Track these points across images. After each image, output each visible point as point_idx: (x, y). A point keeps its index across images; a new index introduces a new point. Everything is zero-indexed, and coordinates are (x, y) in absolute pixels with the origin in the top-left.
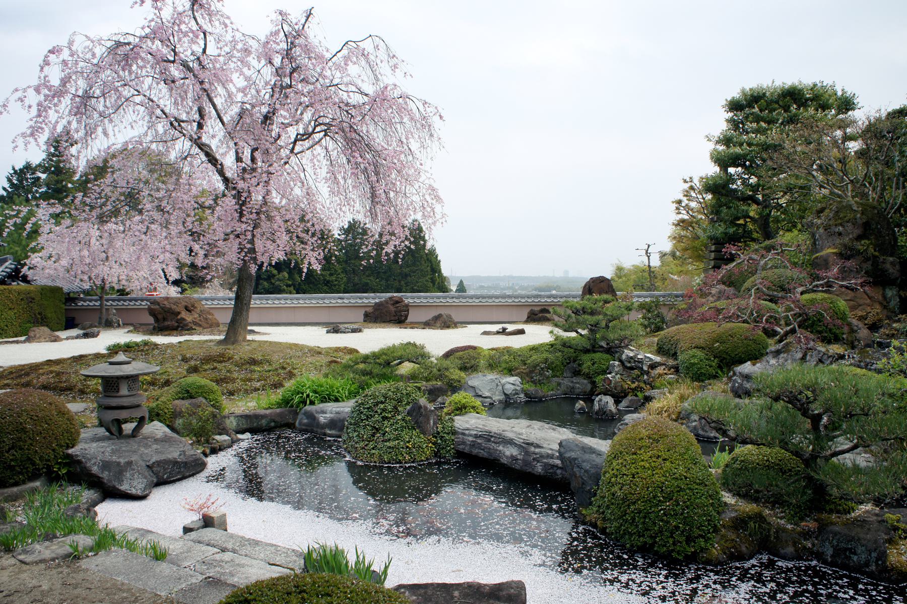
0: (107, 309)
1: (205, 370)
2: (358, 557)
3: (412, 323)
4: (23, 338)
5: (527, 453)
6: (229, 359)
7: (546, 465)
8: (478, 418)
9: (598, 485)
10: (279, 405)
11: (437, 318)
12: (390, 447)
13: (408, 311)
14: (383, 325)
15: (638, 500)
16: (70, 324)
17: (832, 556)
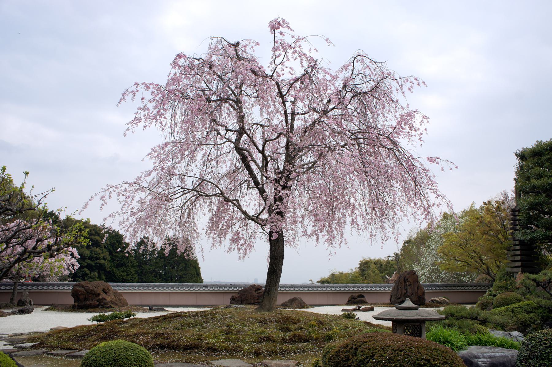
11: (293, 301)
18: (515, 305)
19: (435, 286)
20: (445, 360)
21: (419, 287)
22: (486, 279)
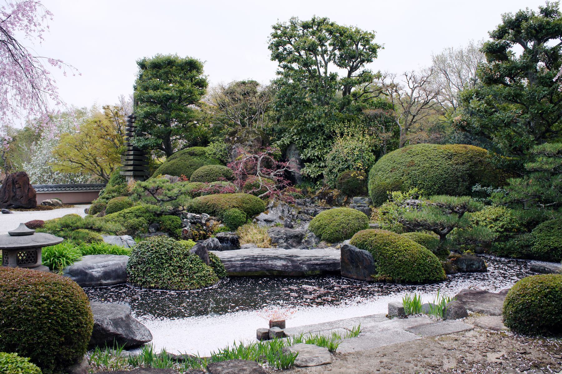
5: (292, 261)
7: (308, 265)
17: (466, 268)
18: (126, 210)
19: (47, 187)
20: (66, 294)
21: (30, 189)
22: (99, 179)
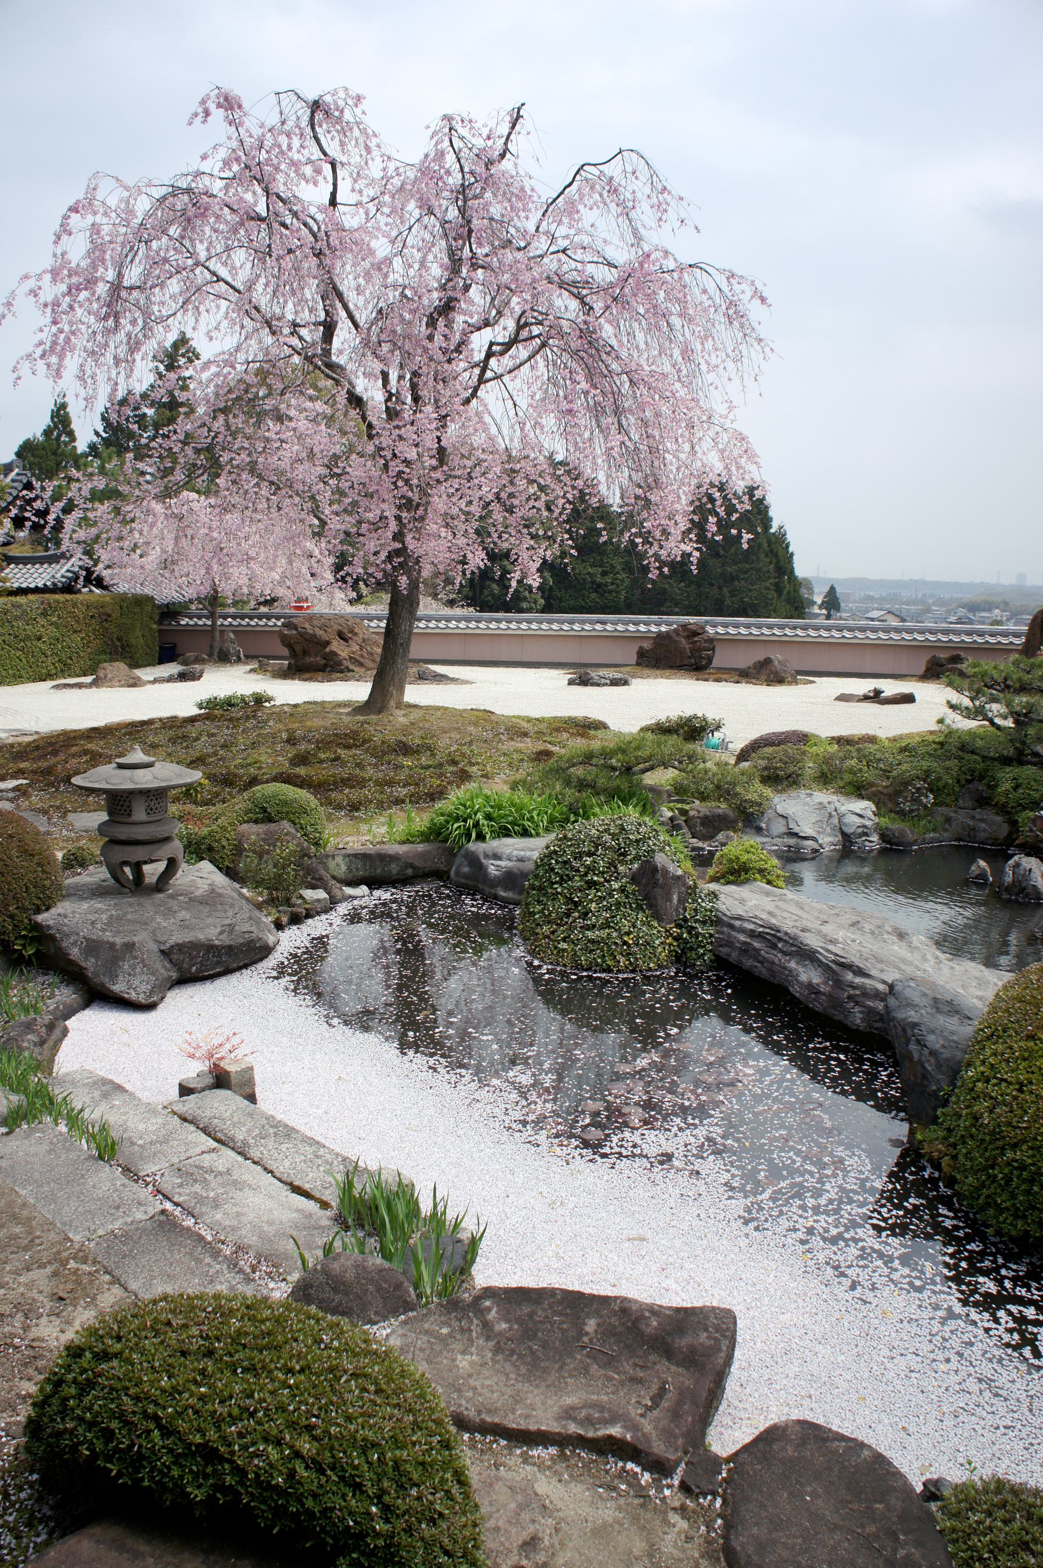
0: (222, 632)
1: (321, 762)
2: (435, 1206)
3: (720, 670)
4: (88, 679)
5: (838, 983)
6: (365, 741)
8: (767, 894)
9: (954, 1086)
10: (425, 837)
12: (593, 941)
13: (713, 649)
14: (667, 672)
15: (1024, 1141)
16: (166, 655)
